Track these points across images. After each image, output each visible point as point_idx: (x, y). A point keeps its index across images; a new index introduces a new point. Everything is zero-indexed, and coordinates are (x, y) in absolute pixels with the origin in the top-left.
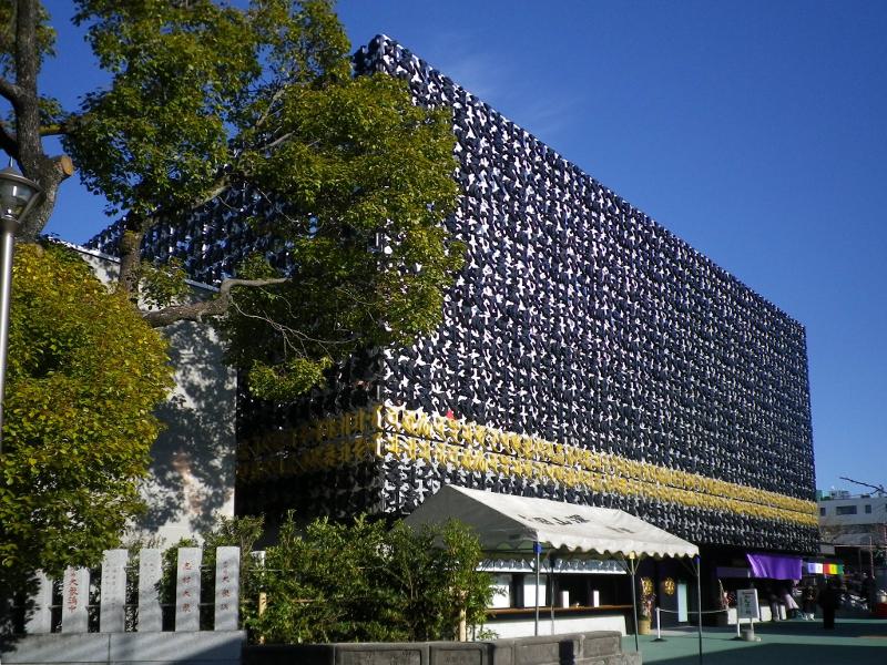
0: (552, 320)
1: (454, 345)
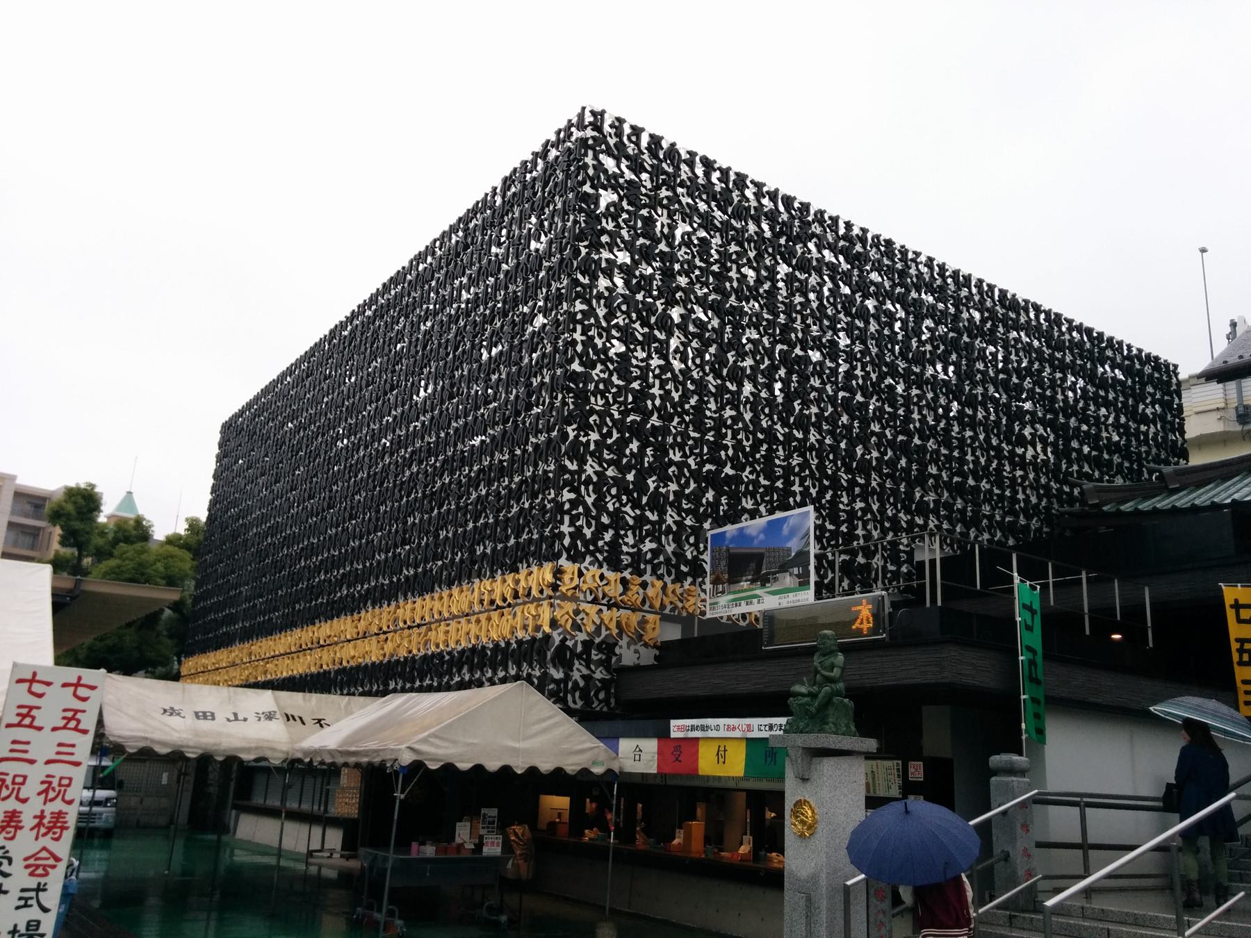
0: (901, 412)
1: (701, 401)
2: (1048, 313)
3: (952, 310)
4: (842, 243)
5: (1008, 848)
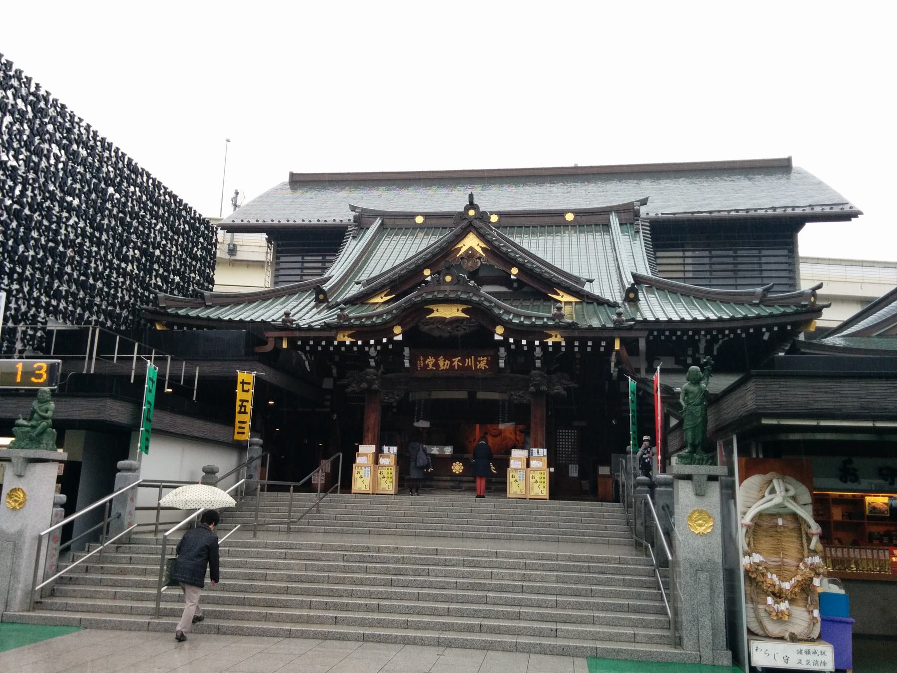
2: (154, 180)
3: (97, 164)
4: (31, 98)
5: (121, 511)
